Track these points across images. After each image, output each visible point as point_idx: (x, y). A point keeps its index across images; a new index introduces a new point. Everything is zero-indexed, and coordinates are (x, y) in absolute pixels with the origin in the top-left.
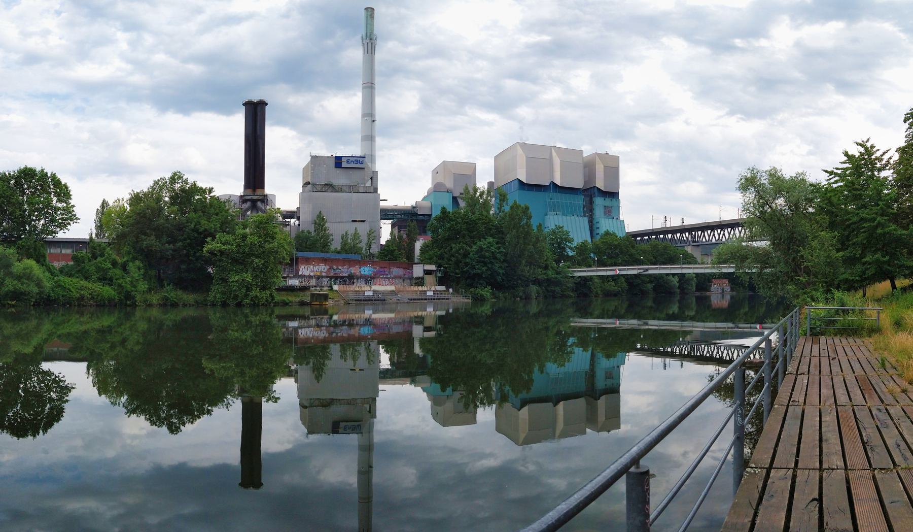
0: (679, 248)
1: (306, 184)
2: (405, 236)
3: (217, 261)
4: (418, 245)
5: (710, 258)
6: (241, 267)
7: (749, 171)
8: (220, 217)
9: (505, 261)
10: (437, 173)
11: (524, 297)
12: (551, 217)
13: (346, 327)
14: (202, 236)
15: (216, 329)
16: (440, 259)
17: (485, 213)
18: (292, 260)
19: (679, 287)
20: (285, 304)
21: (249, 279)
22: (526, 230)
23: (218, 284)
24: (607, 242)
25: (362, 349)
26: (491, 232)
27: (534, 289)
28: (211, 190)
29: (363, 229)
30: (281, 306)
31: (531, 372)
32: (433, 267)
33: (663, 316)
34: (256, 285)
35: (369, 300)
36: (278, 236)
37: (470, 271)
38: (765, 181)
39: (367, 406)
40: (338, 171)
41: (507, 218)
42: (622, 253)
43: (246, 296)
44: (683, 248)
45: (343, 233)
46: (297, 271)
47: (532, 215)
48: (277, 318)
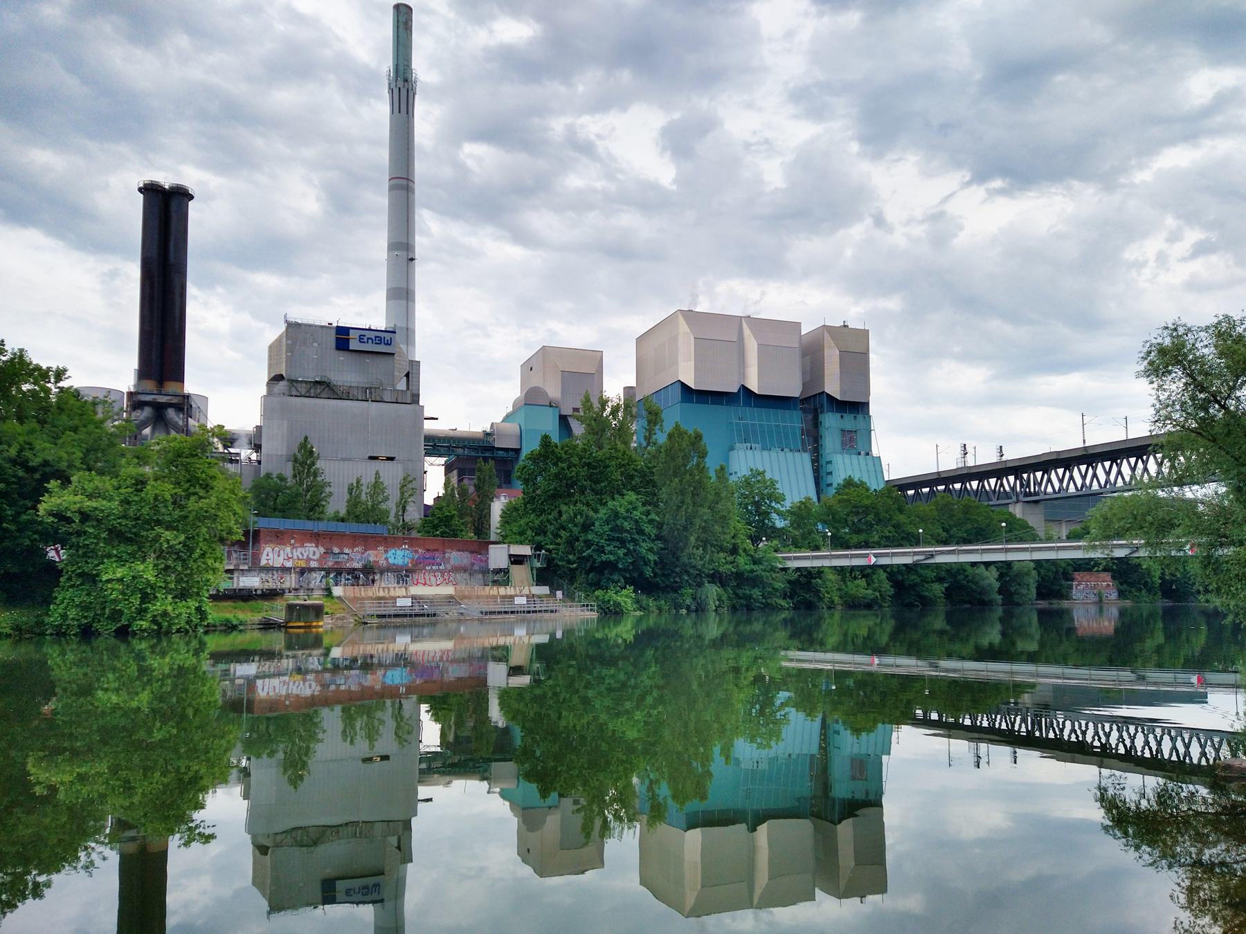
0: (998, 509)
1: (276, 378)
2: (472, 489)
3: (71, 534)
4: (497, 508)
5: (1064, 527)
6: (130, 549)
7: (1166, 333)
8: (82, 437)
9: (659, 537)
10: (531, 369)
11: (693, 607)
12: (741, 453)
13: (358, 672)
14: (37, 476)
15: (65, 690)
16: (539, 534)
17: (621, 446)
18: (246, 533)
19: (1000, 592)
20: (230, 628)
21: (150, 576)
22: (697, 478)
23: (72, 586)
24: (849, 501)
25: (386, 715)
26: (633, 482)
27: (712, 592)
28: (60, 374)
29: (391, 475)
30: (221, 631)
31: (706, 759)
32: (526, 550)
33: (969, 648)
34: (164, 588)
35: (405, 616)
36: (219, 484)
37: (595, 556)
38: (1206, 349)
39: (393, 840)
40: (342, 357)
41: (663, 455)
42: (879, 521)
43: (141, 612)
44: (1002, 508)
45: (350, 481)
46: (256, 558)
47: (708, 448)
48: (210, 659)
